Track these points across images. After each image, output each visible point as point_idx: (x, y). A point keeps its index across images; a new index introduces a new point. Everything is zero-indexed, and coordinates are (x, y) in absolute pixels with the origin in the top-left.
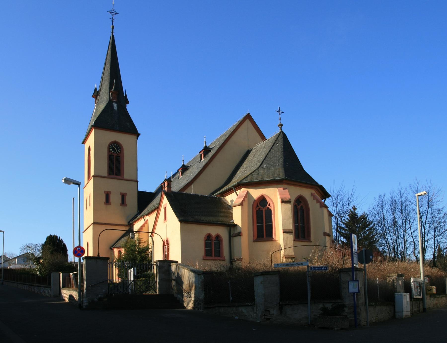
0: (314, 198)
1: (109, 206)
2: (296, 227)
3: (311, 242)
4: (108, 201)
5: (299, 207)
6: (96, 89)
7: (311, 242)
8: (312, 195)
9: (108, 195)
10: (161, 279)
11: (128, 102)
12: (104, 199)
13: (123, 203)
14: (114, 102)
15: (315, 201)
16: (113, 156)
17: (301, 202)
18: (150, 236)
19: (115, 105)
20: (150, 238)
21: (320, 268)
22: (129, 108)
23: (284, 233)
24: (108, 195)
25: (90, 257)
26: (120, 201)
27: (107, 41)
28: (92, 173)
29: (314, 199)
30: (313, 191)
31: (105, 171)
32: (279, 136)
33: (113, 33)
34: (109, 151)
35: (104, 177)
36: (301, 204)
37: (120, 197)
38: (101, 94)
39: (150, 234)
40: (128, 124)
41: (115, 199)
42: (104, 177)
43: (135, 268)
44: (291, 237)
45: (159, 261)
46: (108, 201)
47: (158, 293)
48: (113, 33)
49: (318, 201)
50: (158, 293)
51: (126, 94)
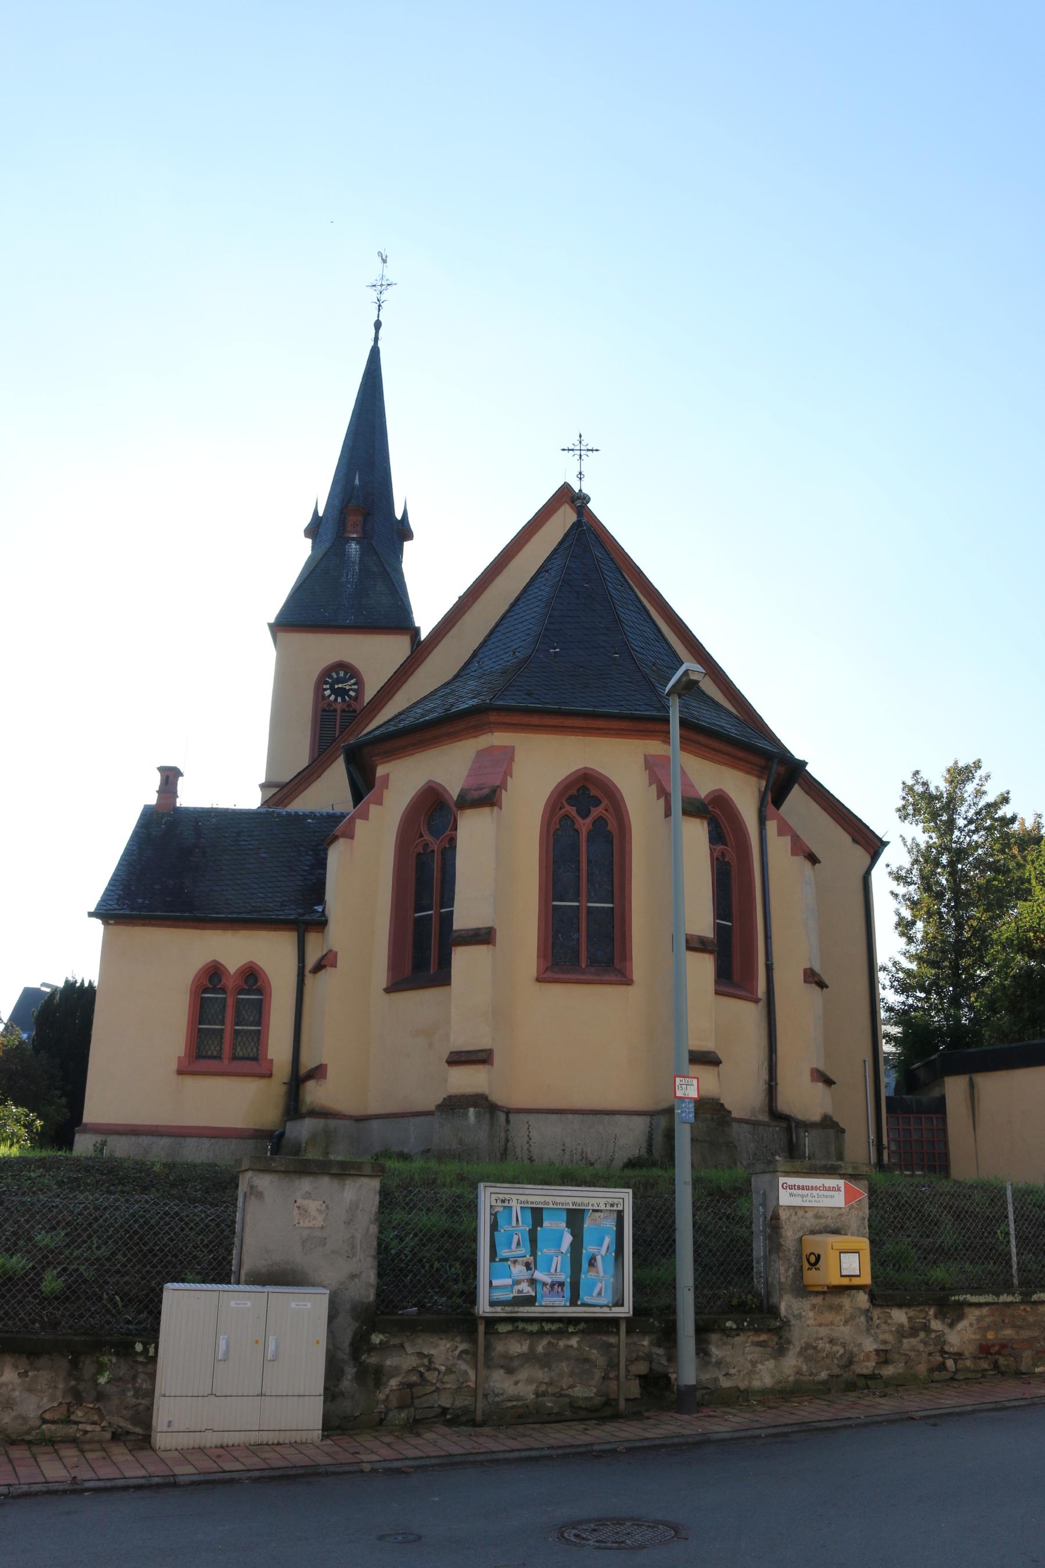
14: (353, 539)
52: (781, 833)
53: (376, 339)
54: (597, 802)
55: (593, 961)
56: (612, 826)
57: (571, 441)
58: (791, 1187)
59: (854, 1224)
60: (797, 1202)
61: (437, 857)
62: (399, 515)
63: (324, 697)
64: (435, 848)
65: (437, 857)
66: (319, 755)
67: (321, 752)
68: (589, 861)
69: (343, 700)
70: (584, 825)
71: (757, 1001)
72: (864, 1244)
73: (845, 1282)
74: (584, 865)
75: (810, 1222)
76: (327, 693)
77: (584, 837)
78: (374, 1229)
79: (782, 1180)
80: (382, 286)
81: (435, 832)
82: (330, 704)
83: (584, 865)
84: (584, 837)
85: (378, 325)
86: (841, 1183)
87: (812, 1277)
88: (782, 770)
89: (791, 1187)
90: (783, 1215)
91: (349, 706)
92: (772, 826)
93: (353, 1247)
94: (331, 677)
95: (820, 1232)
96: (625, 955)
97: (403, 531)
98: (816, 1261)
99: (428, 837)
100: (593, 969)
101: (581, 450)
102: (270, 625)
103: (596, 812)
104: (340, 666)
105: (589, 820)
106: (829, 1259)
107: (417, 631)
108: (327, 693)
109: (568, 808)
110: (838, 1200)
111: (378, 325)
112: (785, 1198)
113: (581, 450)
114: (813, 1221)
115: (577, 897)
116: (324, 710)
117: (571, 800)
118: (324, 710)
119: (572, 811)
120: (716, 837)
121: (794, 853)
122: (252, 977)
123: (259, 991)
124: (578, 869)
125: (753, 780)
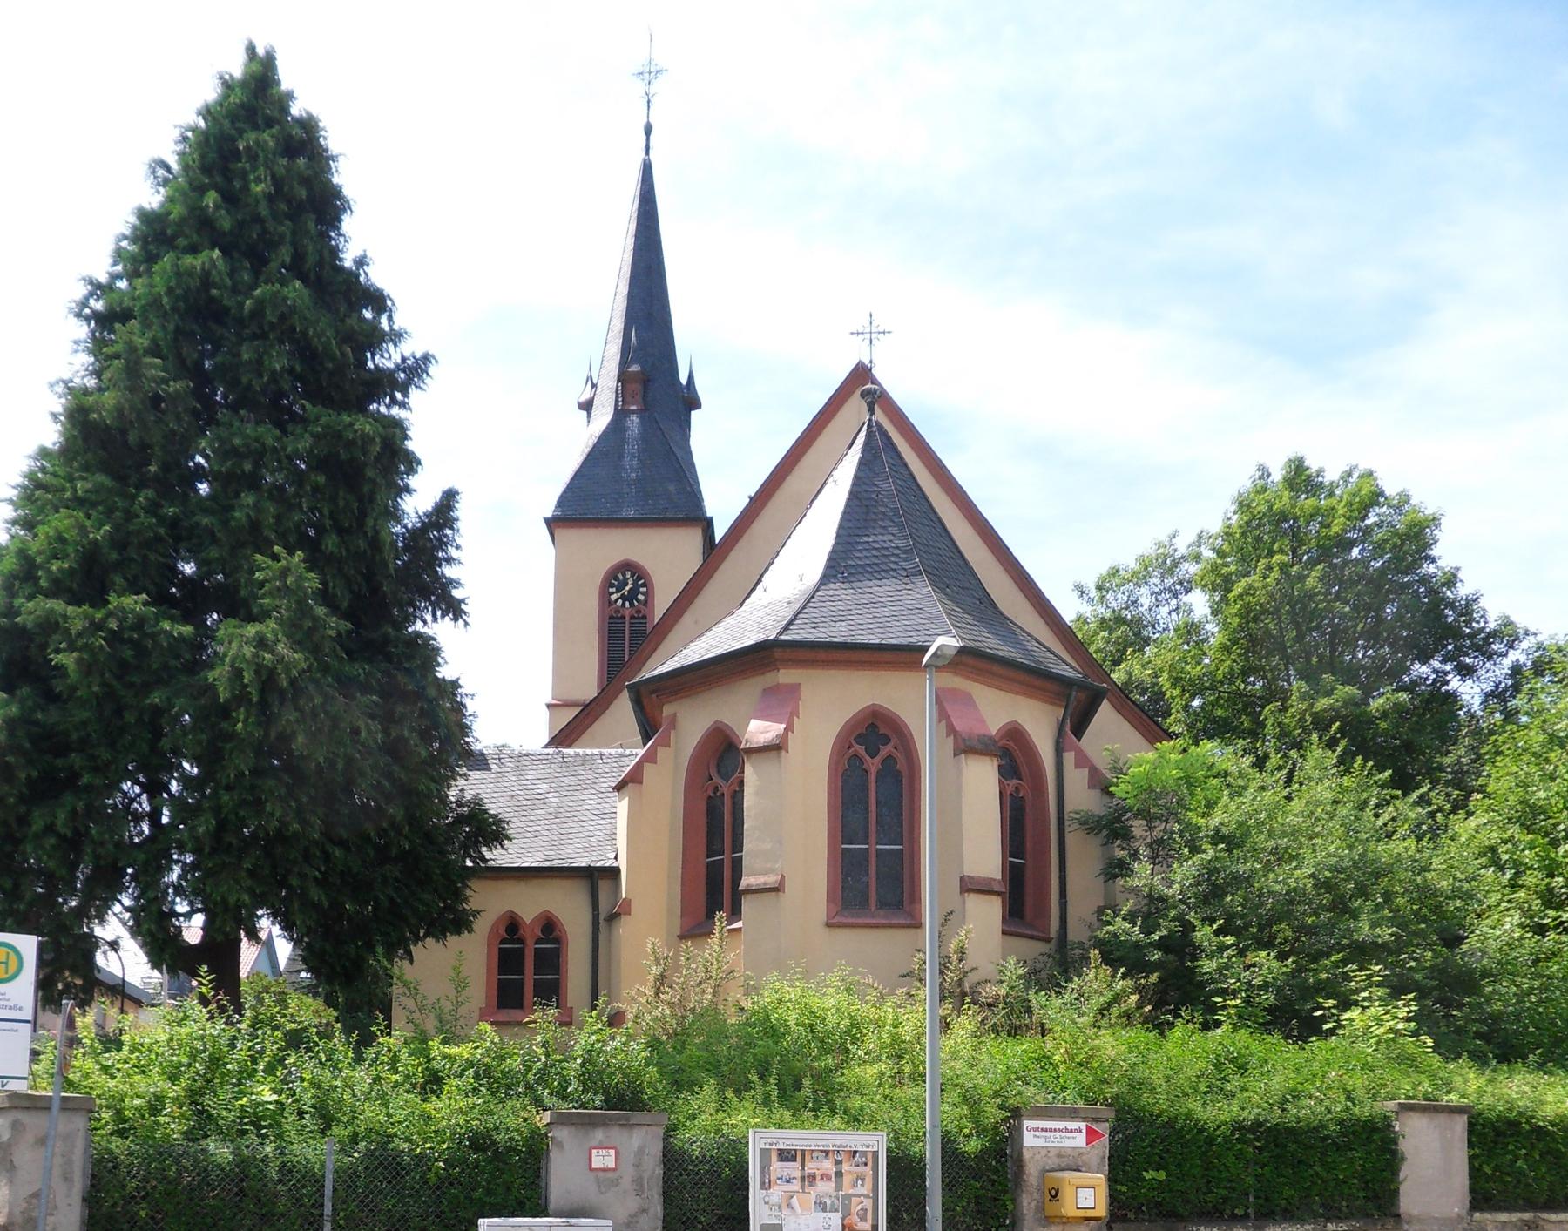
14: (633, 412)
40: (672, 488)
52: (1077, 766)
53: (648, 139)
54: (886, 740)
55: (882, 904)
56: (901, 765)
57: (861, 323)
58: (1035, 1130)
59: (1094, 1161)
60: (1040, 1143)
61: (727, 801)
62: (684, 380)
63: (610, 603)
64: (725, 791)
65: (727, 801)
66: (609, 682)
67: (610, 679)
68: (878, 803)
69: (632, 605)
70: (873, 765)
71: (1048, 940)
72: (1100, 1179)
73: (1082, 1213)
74: (873, 808)
75: (1053, 1162)
76: (614, 597)
77: (872, 777)
78: (659, 1171)
79: (1026, 1123)
80: (650, 74)
81: (726, 778)
82: (617, 611)
83: (873, 808)
84: (872, 777)
85: (648, 130)
86: (1083, 1125)
87: (1051, 1208)
88: (1082, 696)
89: (1035, 1130)
90: (1027, 1155)
91: (638, 611)
92: (1069, 758)
93: (642, 1186)
94: (616, 578)
95: (1063, 1170)
96: (915, 897)
97: (690, 401)
98: (1055, 1195)
99: (717, 779)
100: (882, 912)
101: (871, 334)
102: (548, 521)
103: (885, 751)
104: (627, 566)
105: (878, 759)
106: (1067, 1194)
107: (708, 524)
108: (614, 597)
109: (857, 746)
110: (1080, 1141)
111: (648, 130)
112: (1029, 1139)
113: (871, 334)
114: (1057, 1161)
115: (866, 840)
116: (611, 617)
117: (860, 739)
118: (611, 617)
119: (861, 750)
120: (1009, 770)
121: (1091, 786)
122: (549, 927)
123: (557, 941)
124: (867, 810)
125: (1049, 708)
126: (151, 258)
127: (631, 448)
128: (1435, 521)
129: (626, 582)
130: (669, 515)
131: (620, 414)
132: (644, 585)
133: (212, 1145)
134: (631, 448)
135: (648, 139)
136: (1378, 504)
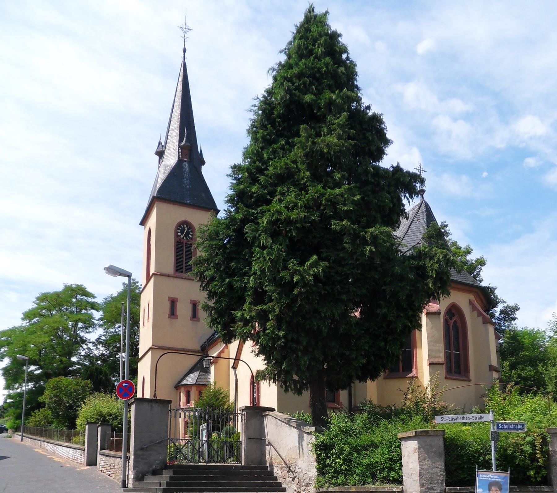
0: (474, 308)
1: (174, 321)
2: (448, 357)
3: (470, 381)
4: (173, 313)
5: (451, 322)
6: (160, 143)
7: (470, 381)
8: (471, 303)
9: (173, 302)
10: (248, 439)
11: (203, 163)
12: (168, 310)
13: (195, 316)
14: (185, 161)
15: (475, 313)
16: (182, 243)
17: (454, 315)
18: (233, 367)
19: (186, 164)
20: (232, 370)
21: (513, 426)
22: (205, 170)
23: (430, 365)
24: (173, 302)
25: (146, 399)
26: (190, 314)
27: (178, 69)
28: (152, 271)
29: (473, 311)
30: (472, 297)
31: (170, 267)
32: (421, 206)
33: (184, 58)
34: (177, 236)
35: (169, 276)
36: (455, 318)
37: (190, 307)
38: (167, 153)
39: (232, 362)
40: (203, 195)
41: (184, 310)
42: (169, 276)
43: (400, 435)
44: (441, 371)
45: (247, 408)
46: (173, 313)
47: (243, 464)
48: (184, 58)
49: (480, 314)
50: (243, 464)
51: (201, 151)
53: (184, 54)
56: (459, 324)
62: (199, 151)
80: (186, 29)
85: (185, 51)
94: (180, 227)
111: (185, 51)
126: (463, 263)
127: (186, 176)
128: (231, 167)
129: (185, 228)
130: (203, 205)
131: (180, 162)
132: (191, 232)
133: (493, 320)
134: (186, 176)
135: (184, 54)
136: (335, 64)
